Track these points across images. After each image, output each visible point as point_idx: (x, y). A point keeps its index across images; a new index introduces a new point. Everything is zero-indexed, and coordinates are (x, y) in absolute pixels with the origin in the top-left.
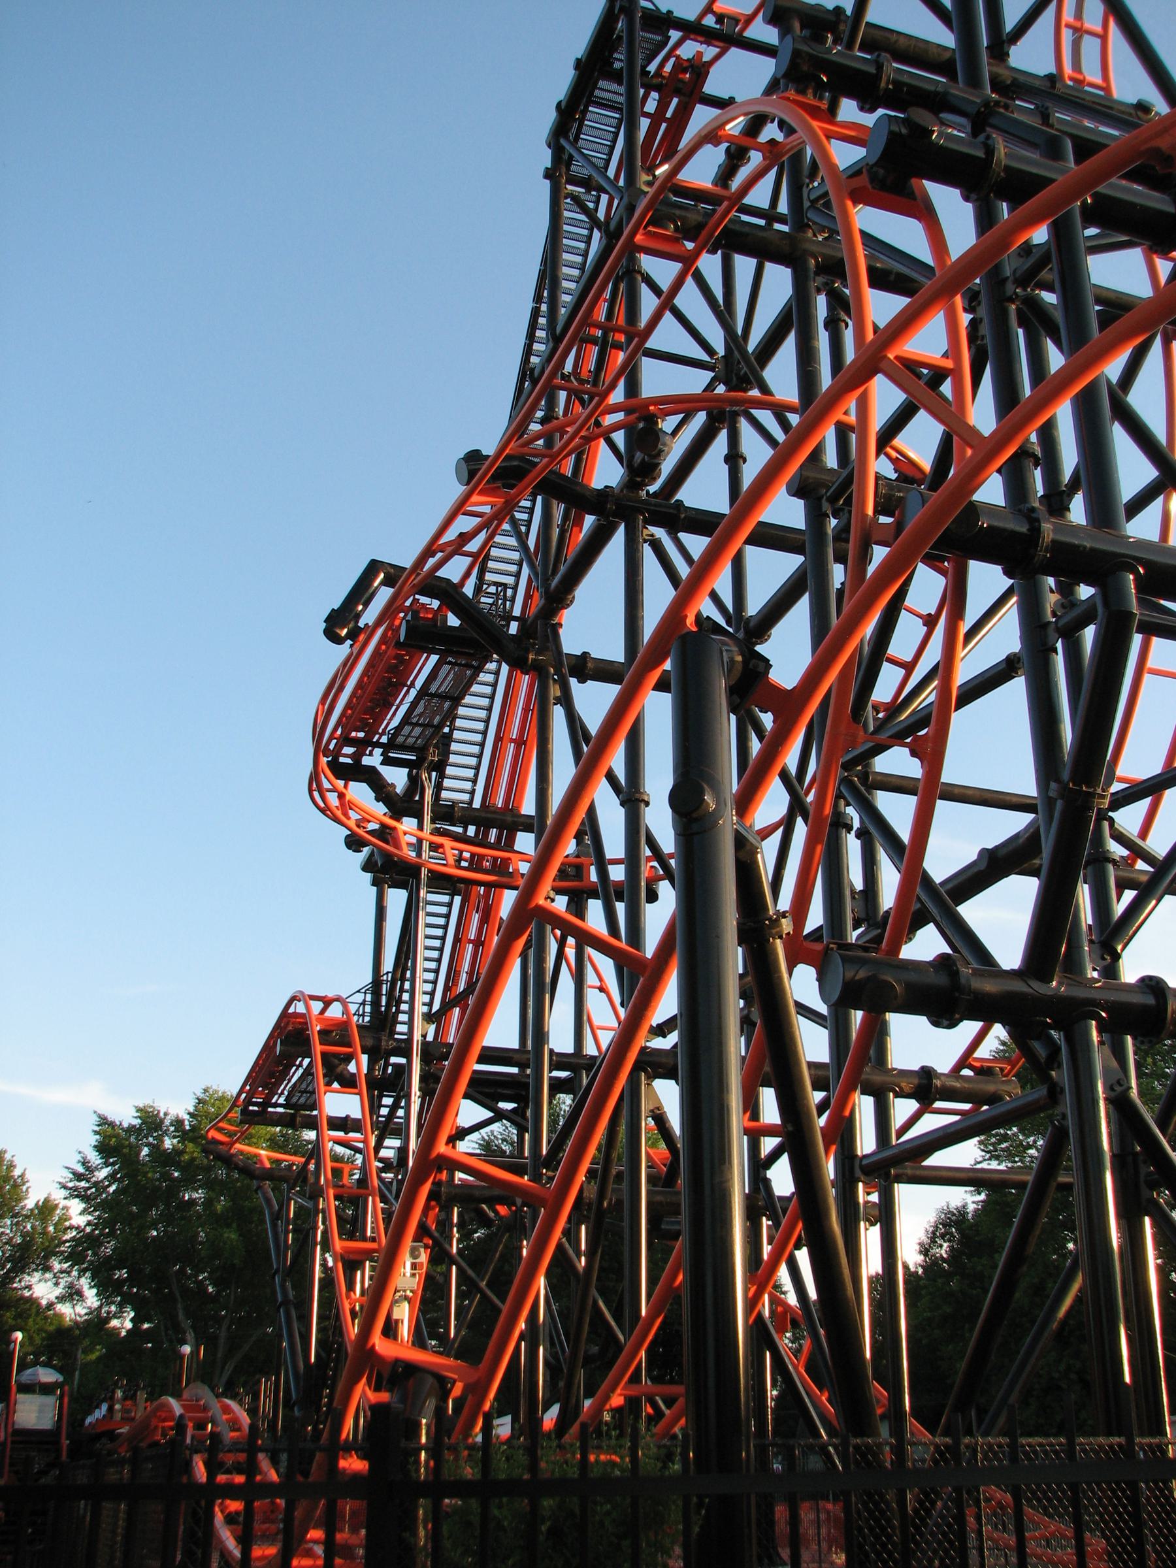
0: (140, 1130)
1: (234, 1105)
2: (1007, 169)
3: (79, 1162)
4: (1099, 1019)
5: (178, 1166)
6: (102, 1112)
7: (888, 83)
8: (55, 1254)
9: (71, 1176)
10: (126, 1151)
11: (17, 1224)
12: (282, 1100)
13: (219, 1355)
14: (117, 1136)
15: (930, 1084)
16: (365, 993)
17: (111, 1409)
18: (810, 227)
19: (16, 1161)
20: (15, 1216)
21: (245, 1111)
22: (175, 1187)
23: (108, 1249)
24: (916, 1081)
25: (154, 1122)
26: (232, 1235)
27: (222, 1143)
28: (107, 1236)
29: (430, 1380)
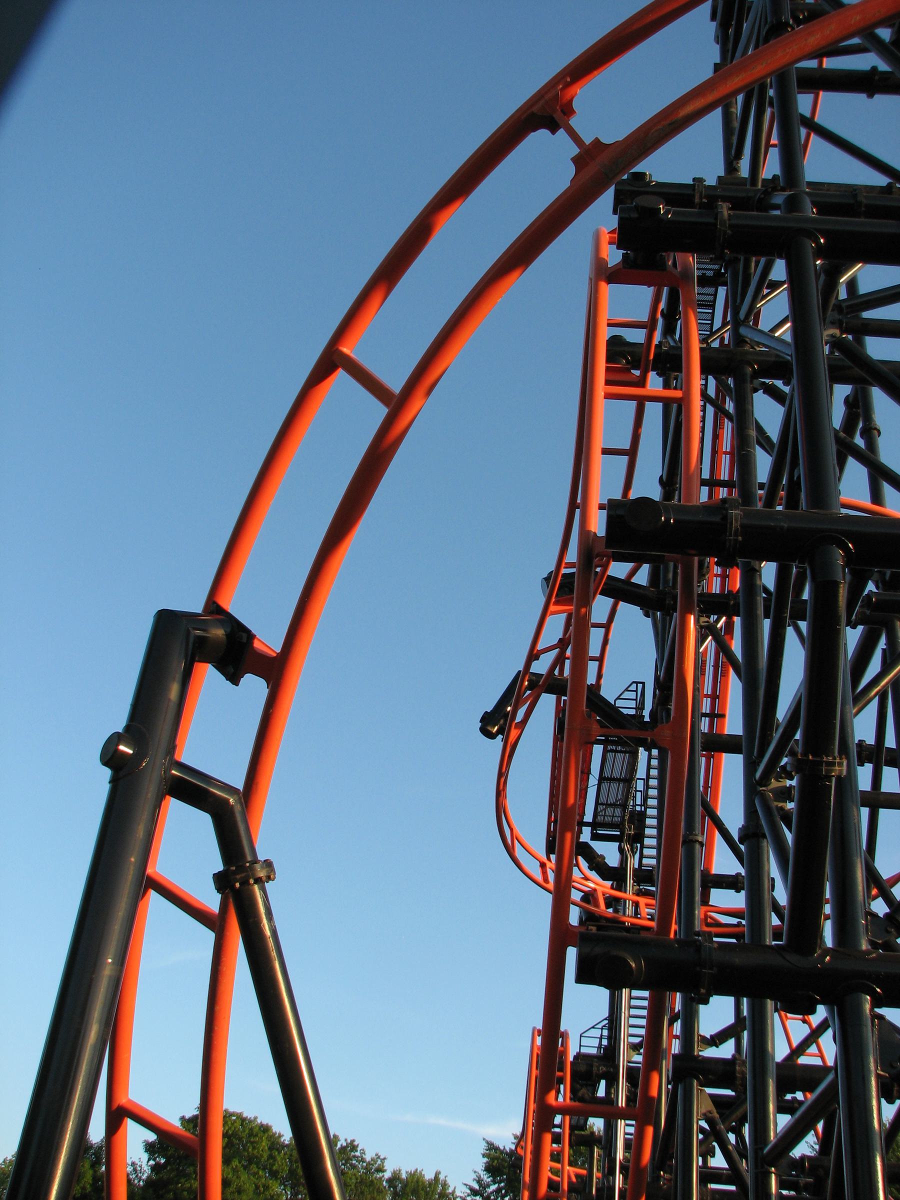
2: (731, 226)
3: (474, 1179)
6: (489, 1139)
7: (701, 198)
9: (469, 1191)
16: (602, 1029)
18: (747, 342)
19: (449, 1181)
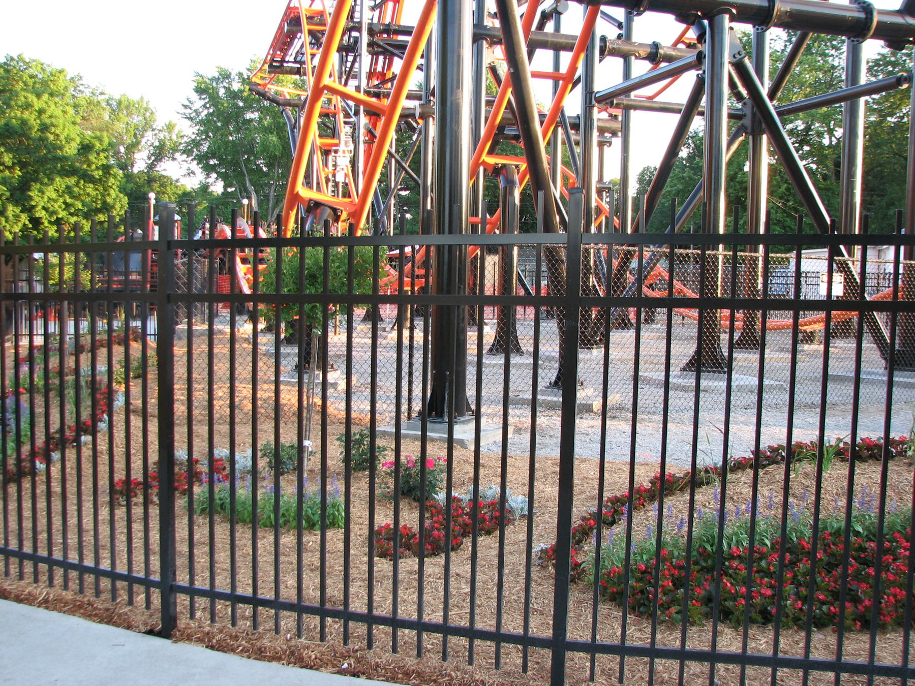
0: (219, 78)
1: (265, 62)
4: (731, 14)
5: (242, 99)
8: (177, 151)
10: (211, 91)
11: (155, 135)
12: (292, 59)
13: (270, 206)
14: (205, 83)
15: (657, 53)
17: (204, 233)
20: (153, 130)
21: (271, 66)
22: (240, 112)
23: (205, 148)
24: (649, 50)
25: (226, 74)
26: (274, 138)
27: (259, 85)
28: (205, 139)
29: (329, 211)
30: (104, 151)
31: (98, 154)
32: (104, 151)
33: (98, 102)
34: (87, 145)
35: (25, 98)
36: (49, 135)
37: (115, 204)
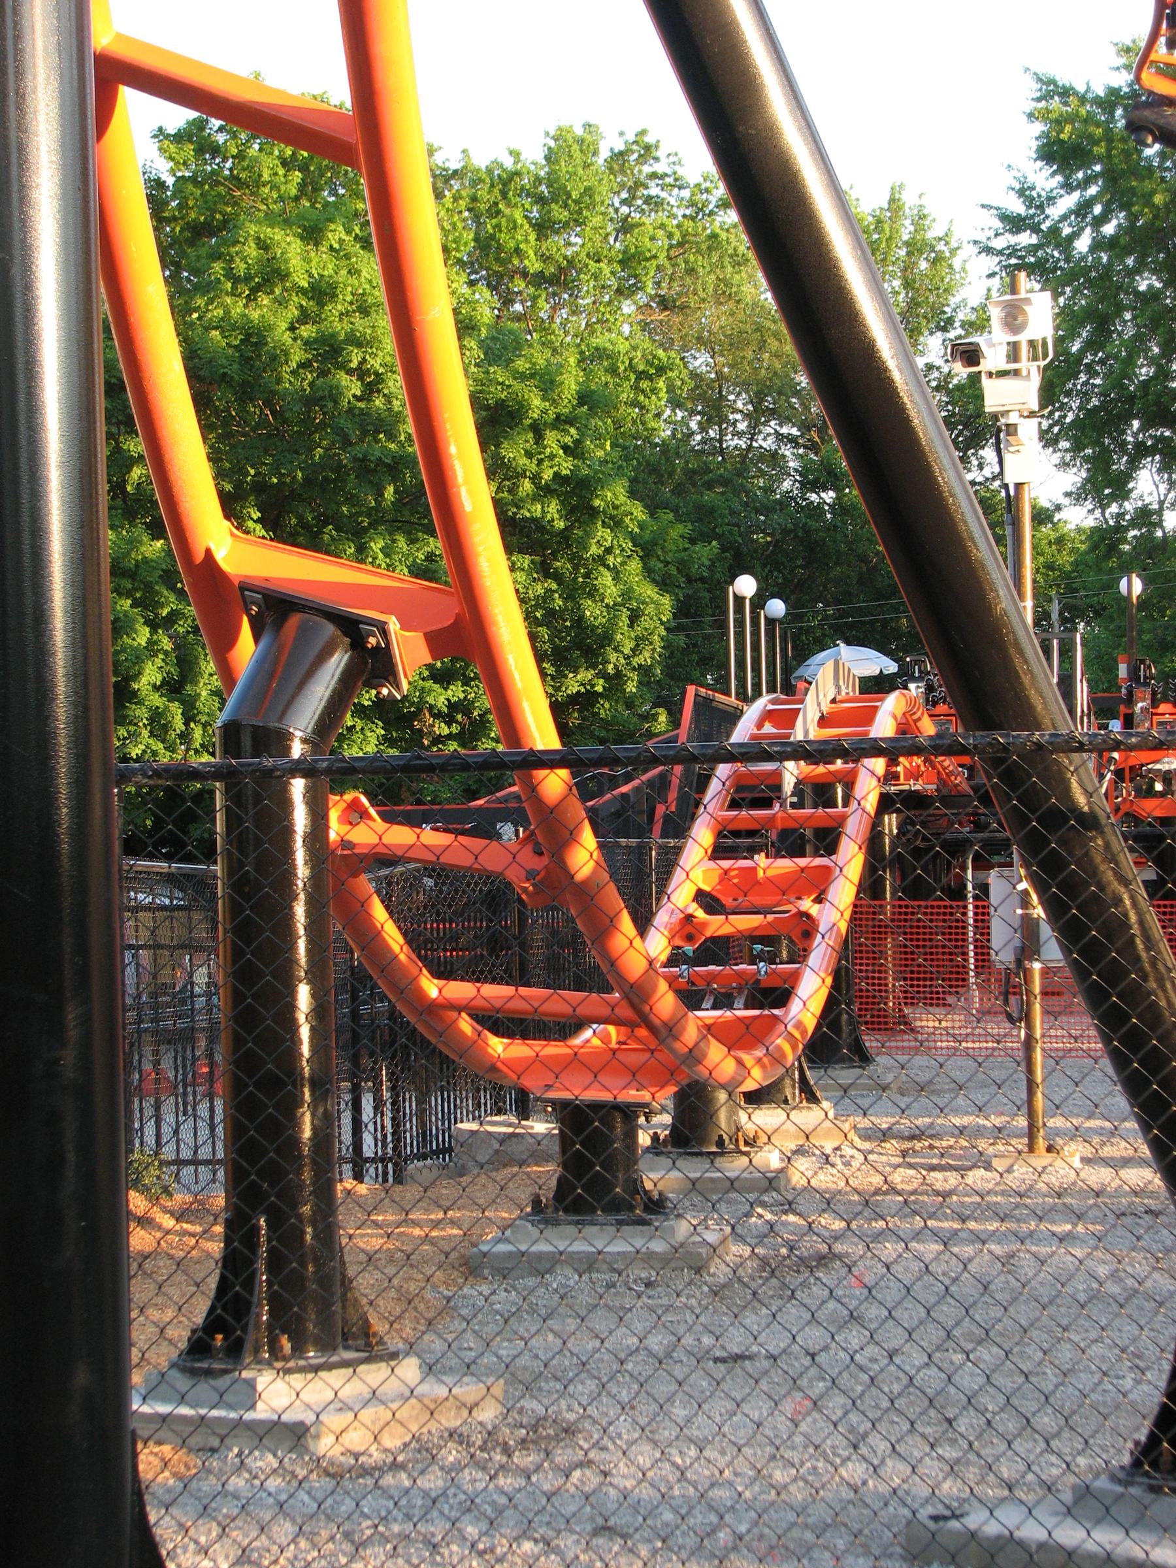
30: (560, 422)
31: (539, 438)
32: (560, 422)
33: (714, 236)
34: (501, 404)
35: (263, 245)
36: (344, 379)
37: (613, 621)
